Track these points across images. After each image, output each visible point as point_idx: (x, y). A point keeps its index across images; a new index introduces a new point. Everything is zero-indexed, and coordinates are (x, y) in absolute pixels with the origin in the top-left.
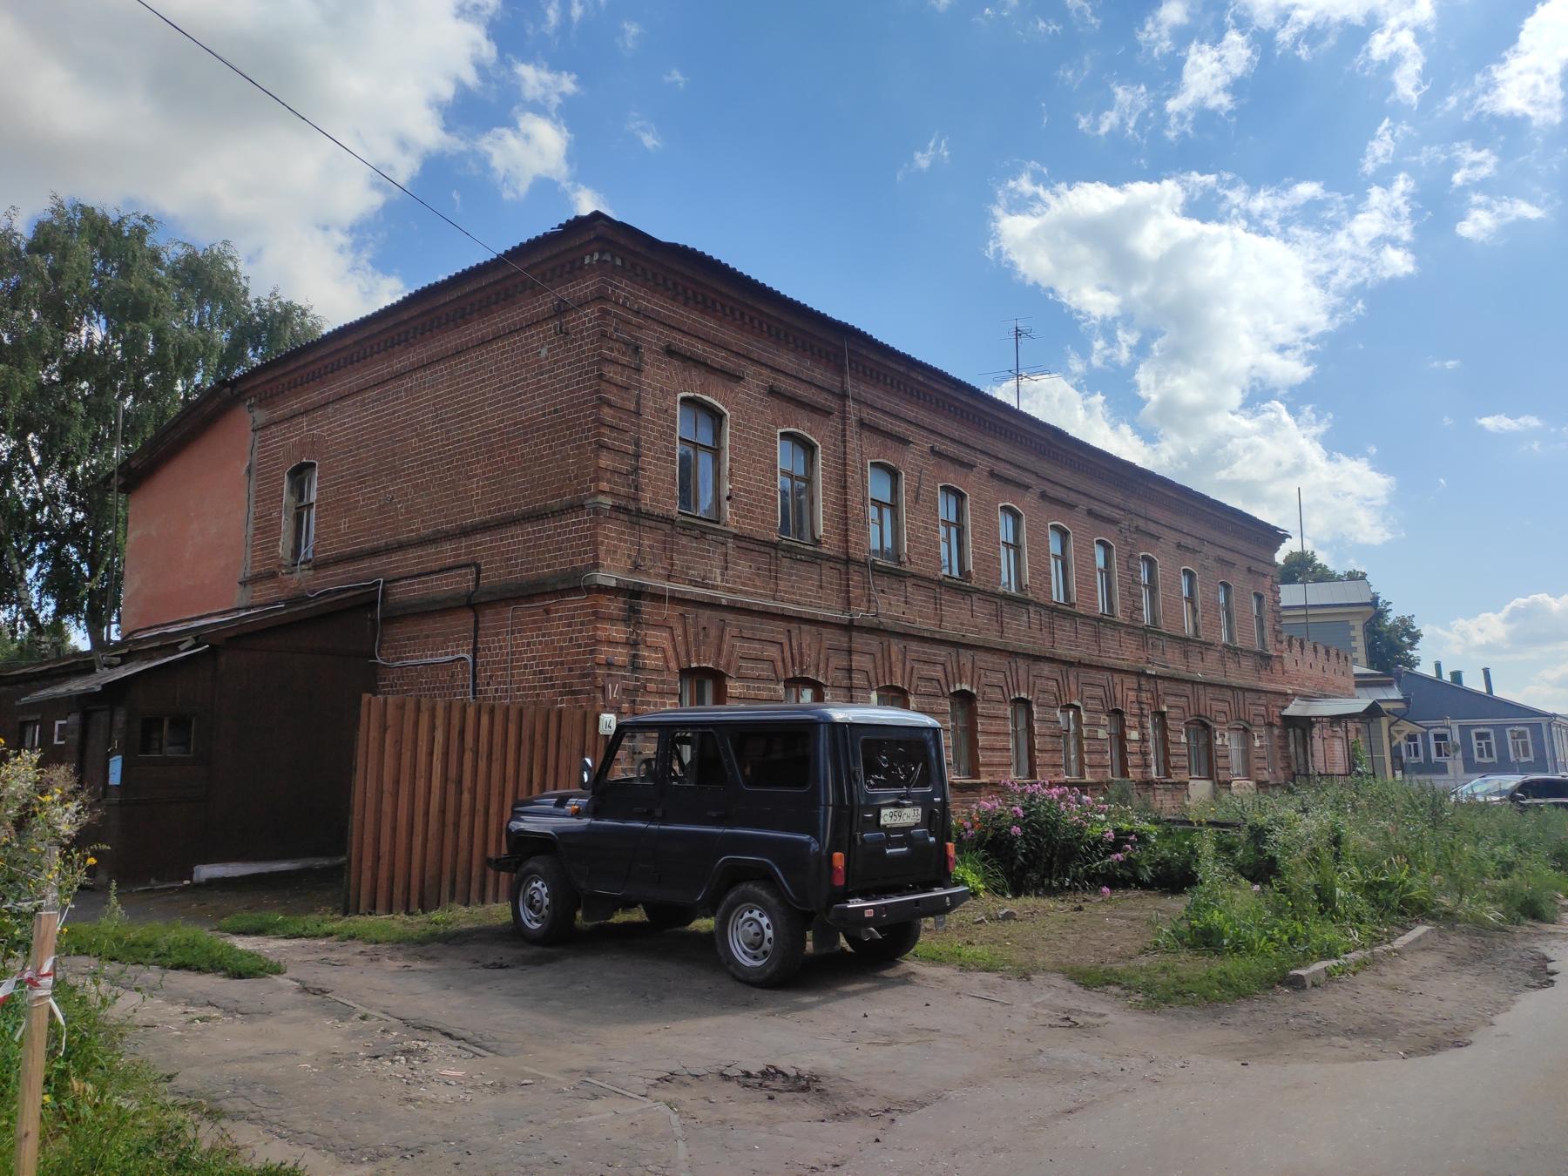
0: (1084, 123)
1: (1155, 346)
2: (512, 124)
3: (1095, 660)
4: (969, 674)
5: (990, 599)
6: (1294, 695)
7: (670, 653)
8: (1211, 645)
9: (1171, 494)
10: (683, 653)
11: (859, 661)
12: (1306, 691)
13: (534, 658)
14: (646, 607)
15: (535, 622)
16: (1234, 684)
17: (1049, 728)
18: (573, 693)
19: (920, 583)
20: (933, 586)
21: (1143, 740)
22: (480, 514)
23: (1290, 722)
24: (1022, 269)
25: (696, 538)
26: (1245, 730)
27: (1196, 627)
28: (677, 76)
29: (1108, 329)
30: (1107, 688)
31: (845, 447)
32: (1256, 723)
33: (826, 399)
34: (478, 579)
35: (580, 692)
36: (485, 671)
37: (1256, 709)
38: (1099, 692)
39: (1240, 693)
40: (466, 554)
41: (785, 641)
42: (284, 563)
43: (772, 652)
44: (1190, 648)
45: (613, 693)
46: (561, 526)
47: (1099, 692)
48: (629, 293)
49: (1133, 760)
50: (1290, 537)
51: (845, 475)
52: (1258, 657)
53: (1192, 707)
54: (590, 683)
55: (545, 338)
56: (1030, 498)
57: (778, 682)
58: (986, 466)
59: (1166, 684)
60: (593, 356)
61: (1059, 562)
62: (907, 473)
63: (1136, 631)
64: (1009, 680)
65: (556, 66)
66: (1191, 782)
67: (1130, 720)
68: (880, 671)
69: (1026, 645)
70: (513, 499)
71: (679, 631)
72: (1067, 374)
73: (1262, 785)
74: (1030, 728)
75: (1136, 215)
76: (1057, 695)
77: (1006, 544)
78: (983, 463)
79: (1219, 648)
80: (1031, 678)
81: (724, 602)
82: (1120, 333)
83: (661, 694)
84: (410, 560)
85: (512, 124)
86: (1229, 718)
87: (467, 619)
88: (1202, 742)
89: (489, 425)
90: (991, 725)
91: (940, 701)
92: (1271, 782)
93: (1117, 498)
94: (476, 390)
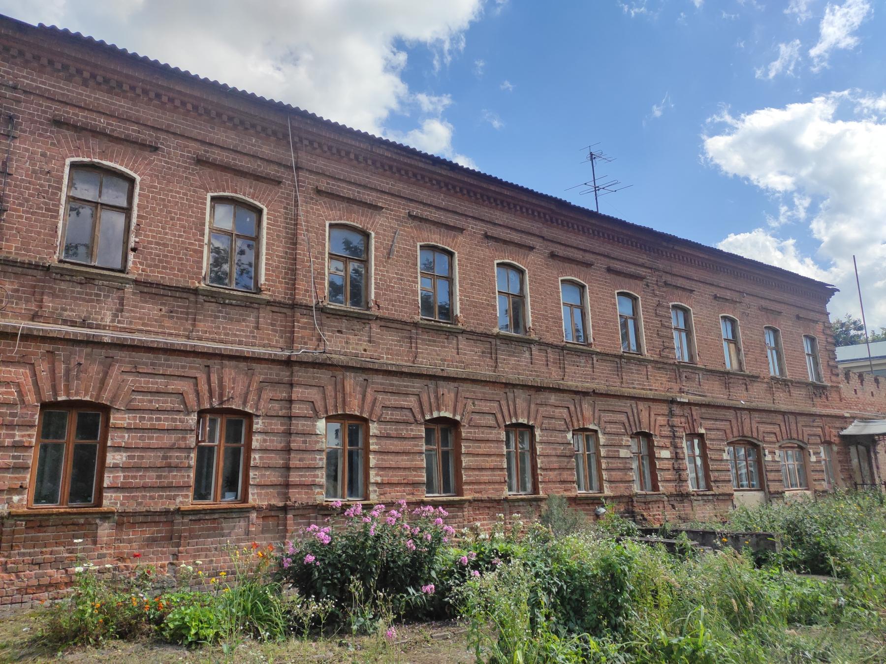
0: (759, 74)
1: (821, 206)
2: (419, 127)
6: (854, 418)
8: (758, 377)
12: (867, 414)
16: (782, 410)
20: (408, 328)
23: (849, 441)
24: (724, 168)
25: (81, 284)
27: (740, 363)
28: (507, 84)
29: (788, 198)
37: (806, 431)
39: (792, 418)
50: (838, 290)
52: (811, 388)
53: (735, 430)
57: (188, 413)
58: (480, 230)
59: (703, 410)
61: (774, 352)
62: (377, 233)
65: (439, 93)
72: (767, 228)
73: (820, 494)
75: (799, 125)
76: (568, 420)
77: (808, 354)
78: (601, 263)
79: (766, 380)
80: (533, 406)
81: (107, 340)
82: (797, 202)
85: (419, 127)
86: (779, 438)
91: (413, 427)
93: (643, 259)
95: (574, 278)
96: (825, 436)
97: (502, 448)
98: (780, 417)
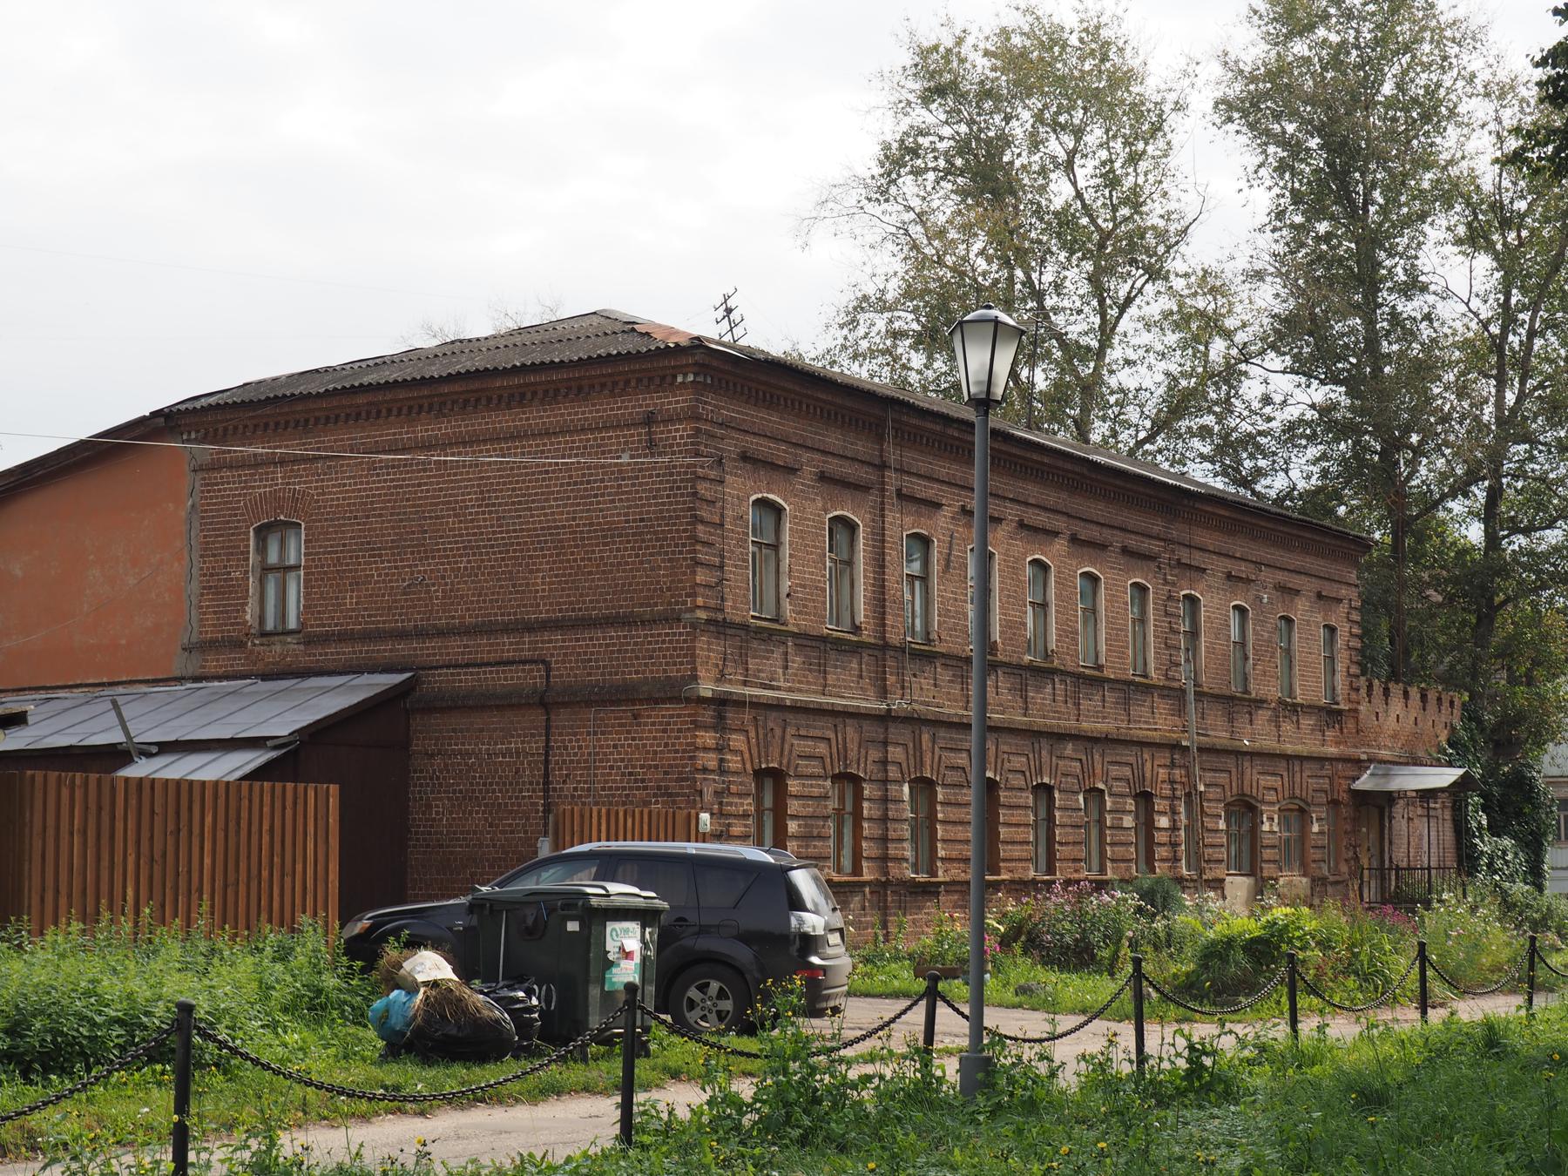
3: (1124, 734)
4: (993, 760)
5: (1016, 671)
6: (1370, 761)
7: (747, 756)
8: (1263, 701)
9: (1222, 512)
10: (755, 755)
11: (895, 753)
13: (622, 760)
14: (731, 715)
15: (621, 725)
17: (1071, 817)
18: (670, 795)
19: (948, 662)
20: (960, 664)
21: (1174, 828)
22: (547, 612)
23: (1363, 799)
26: (1302, 811)
30: (1135, 766)
31: (883, 522)
32: (1316, 801)
33: (867, 473)
34: (548, 676)
35: (678, 795)
36: (561, 769)
38: (1127, 771)
39: (1297, 763)
40: (529, 650)
41: (832, 736)
42: (252, 631)
43: (822, 749)
44: (1236, 709)
45: (708, 796)
46: (652, 636)
47: (1127, 771)
48: (715, 406)
49: (1161, 852)
51: (883, 553)
52: (1323, 714)
53: (1234, 784)
54: (689, 787)
55: (626, 443)
56: (1060, 545)
60: (686, 473)
63: (1172, 693)
64: (1032, 763)
66: (1229, 879)
67: (1160, 804)
68: (912, 762)
69: (1052, 723)
70: (591, 602)
71: (752, 734)
74: (1050, 818)
78: (810, 465)
81: (788, 703)
83: (740, 795)
84: (455, 648)
87: (538, 717)
88: (1246, 826)
89: (555, 521)
90: (1013, 815)
92: (1332, 879)
93: (1157, 526)
94: (537, 480)
95: (845, 513)
96: (1332, 791)
97: (1028, 816)
98: (1284, 764)
